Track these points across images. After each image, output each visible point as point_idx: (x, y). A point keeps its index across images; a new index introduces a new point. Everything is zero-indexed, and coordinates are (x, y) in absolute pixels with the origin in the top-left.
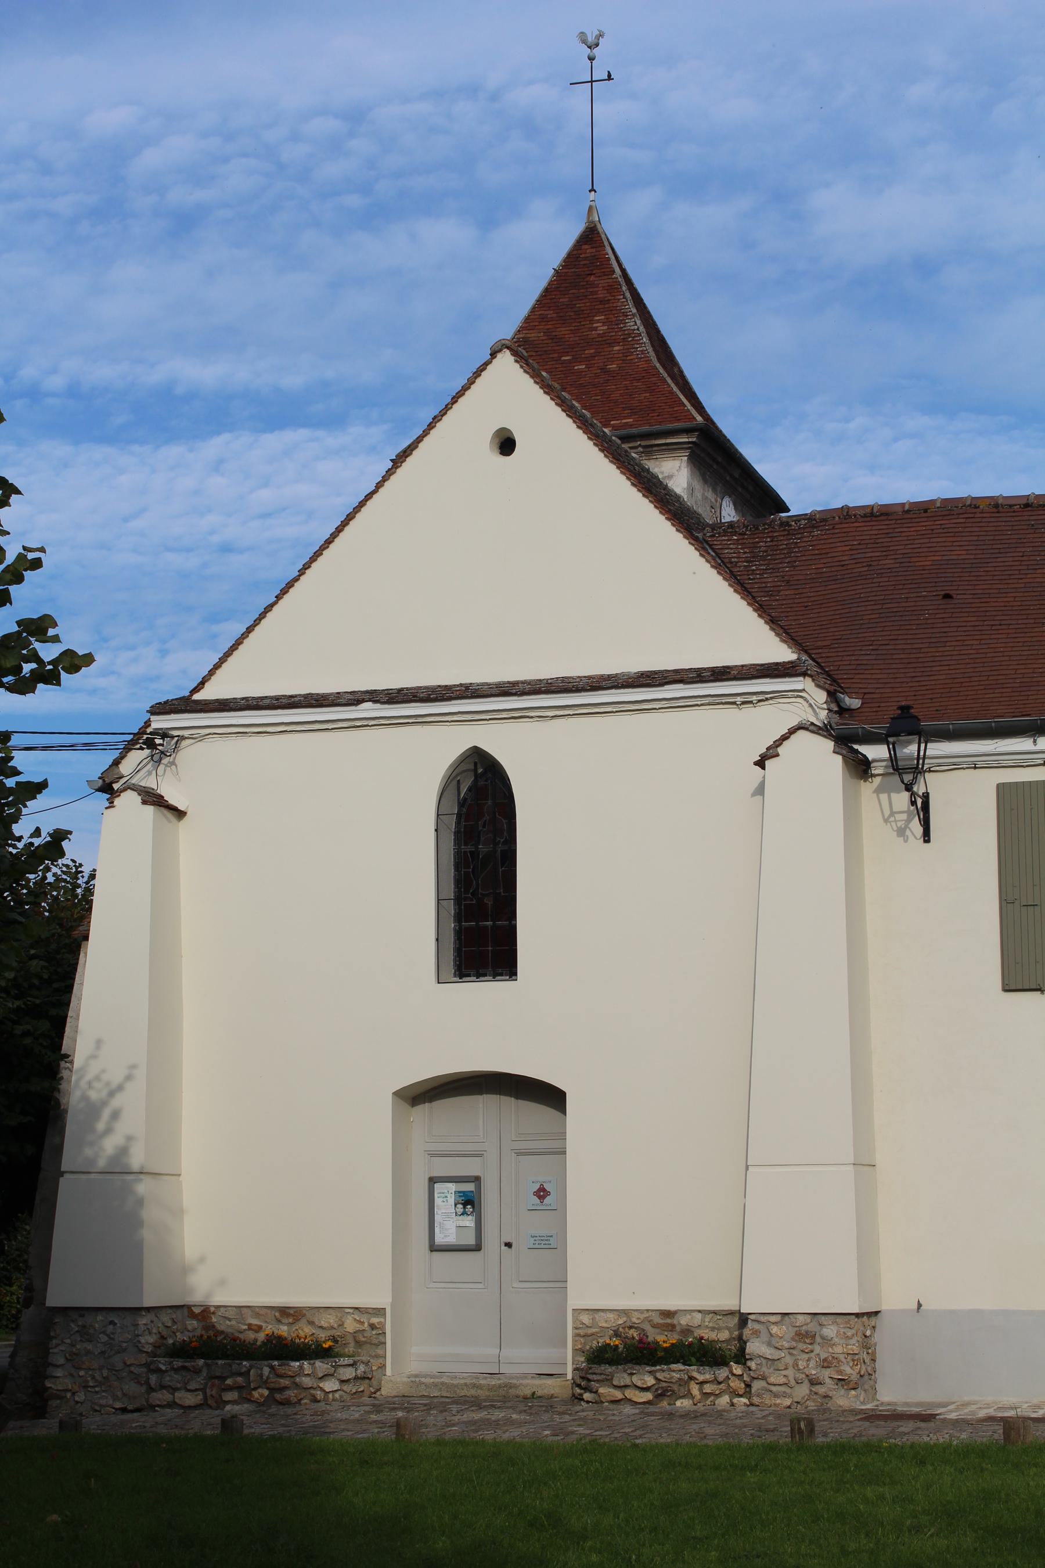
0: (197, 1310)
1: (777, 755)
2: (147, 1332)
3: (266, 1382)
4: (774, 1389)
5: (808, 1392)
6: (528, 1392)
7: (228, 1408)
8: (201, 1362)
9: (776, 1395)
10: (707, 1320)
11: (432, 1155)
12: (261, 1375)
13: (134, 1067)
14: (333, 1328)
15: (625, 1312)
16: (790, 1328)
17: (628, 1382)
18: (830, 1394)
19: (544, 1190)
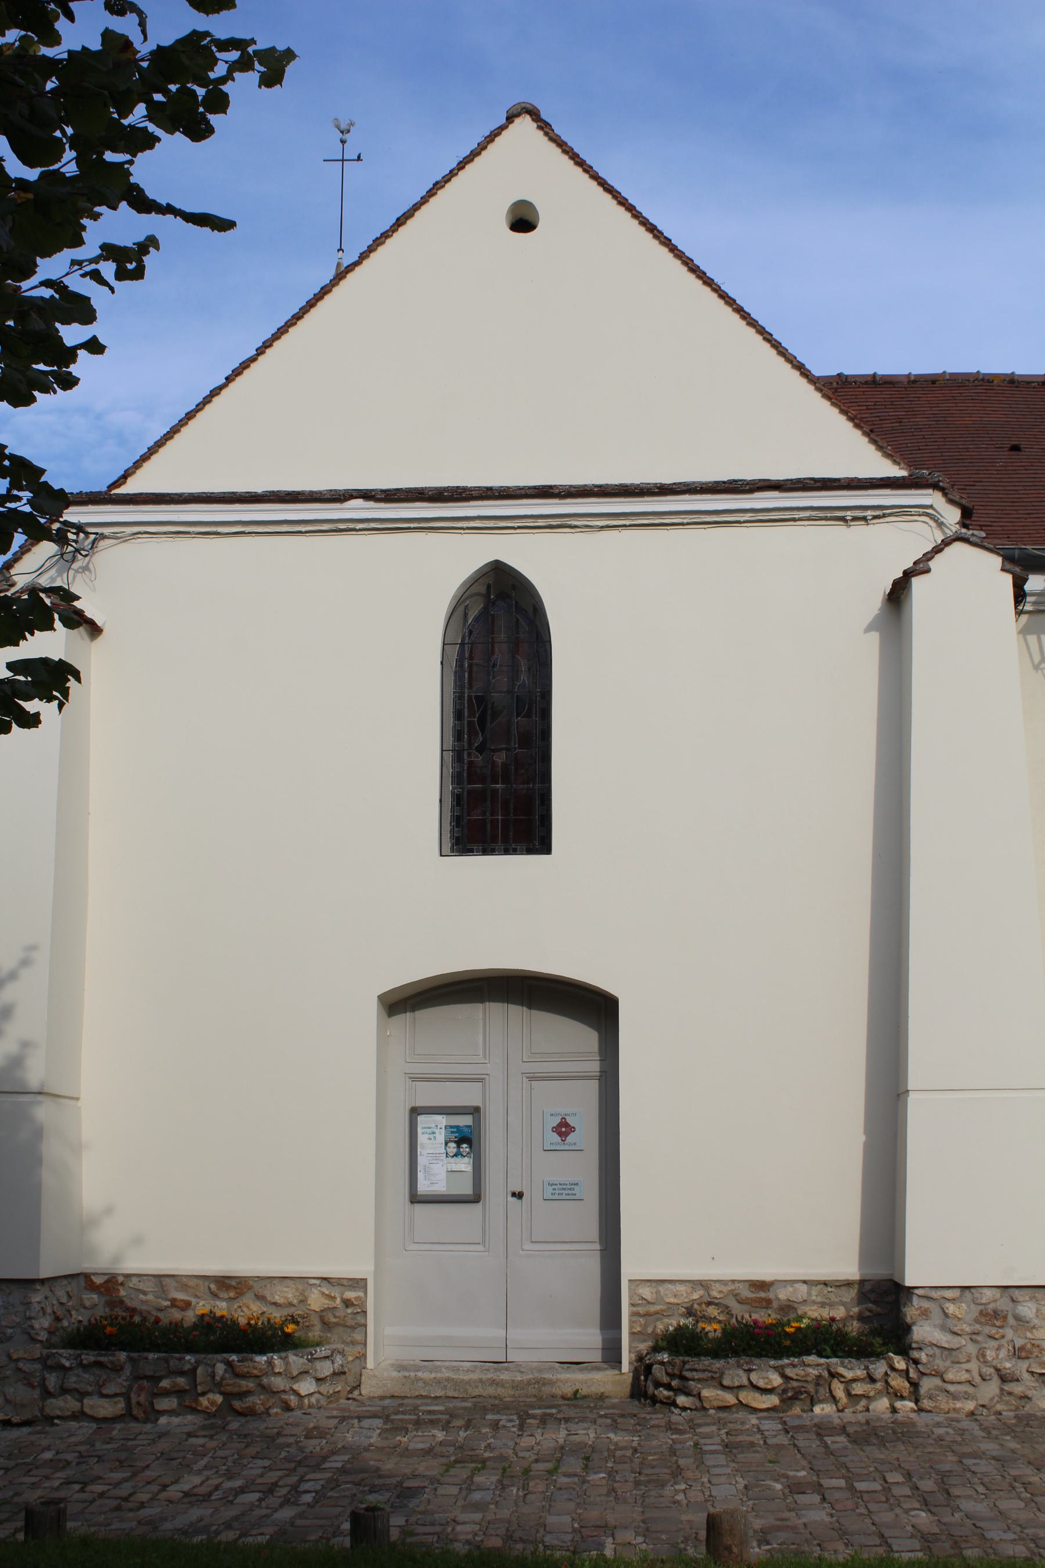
0: (98, 1280)
1: (928, 571)
2: (41, 1314)
3: (220, 1384)
4: (951, 1388)
5: (997, 1391)
6: (568, 1390)
7: (163, 1420)
8: (123, 1356)
9: (955, 1397)
10: (814, 1293)
11: (414, 1079)
12: (213, 1375)
13: (33, 948)
14: (291, 1304)
15: (704, 1284)
16: (972, 1306)
17: (745, 1382)
18: (1029, 1393)
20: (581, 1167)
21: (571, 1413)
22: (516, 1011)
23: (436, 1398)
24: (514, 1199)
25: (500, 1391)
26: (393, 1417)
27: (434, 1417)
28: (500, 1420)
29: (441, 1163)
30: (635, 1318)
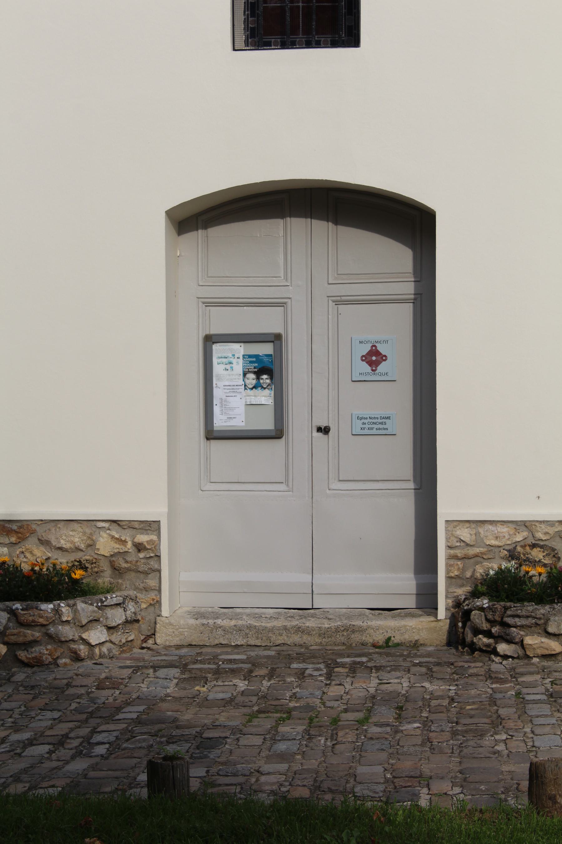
6: (380, 638)
11: (208, 304)
14: (78, 549)
15: (526, 525)
22: (321, 228)
23: (237, 646)
24: (320, 434)
25: (306, 639)
29: (239, 396)
30: (452, 562)
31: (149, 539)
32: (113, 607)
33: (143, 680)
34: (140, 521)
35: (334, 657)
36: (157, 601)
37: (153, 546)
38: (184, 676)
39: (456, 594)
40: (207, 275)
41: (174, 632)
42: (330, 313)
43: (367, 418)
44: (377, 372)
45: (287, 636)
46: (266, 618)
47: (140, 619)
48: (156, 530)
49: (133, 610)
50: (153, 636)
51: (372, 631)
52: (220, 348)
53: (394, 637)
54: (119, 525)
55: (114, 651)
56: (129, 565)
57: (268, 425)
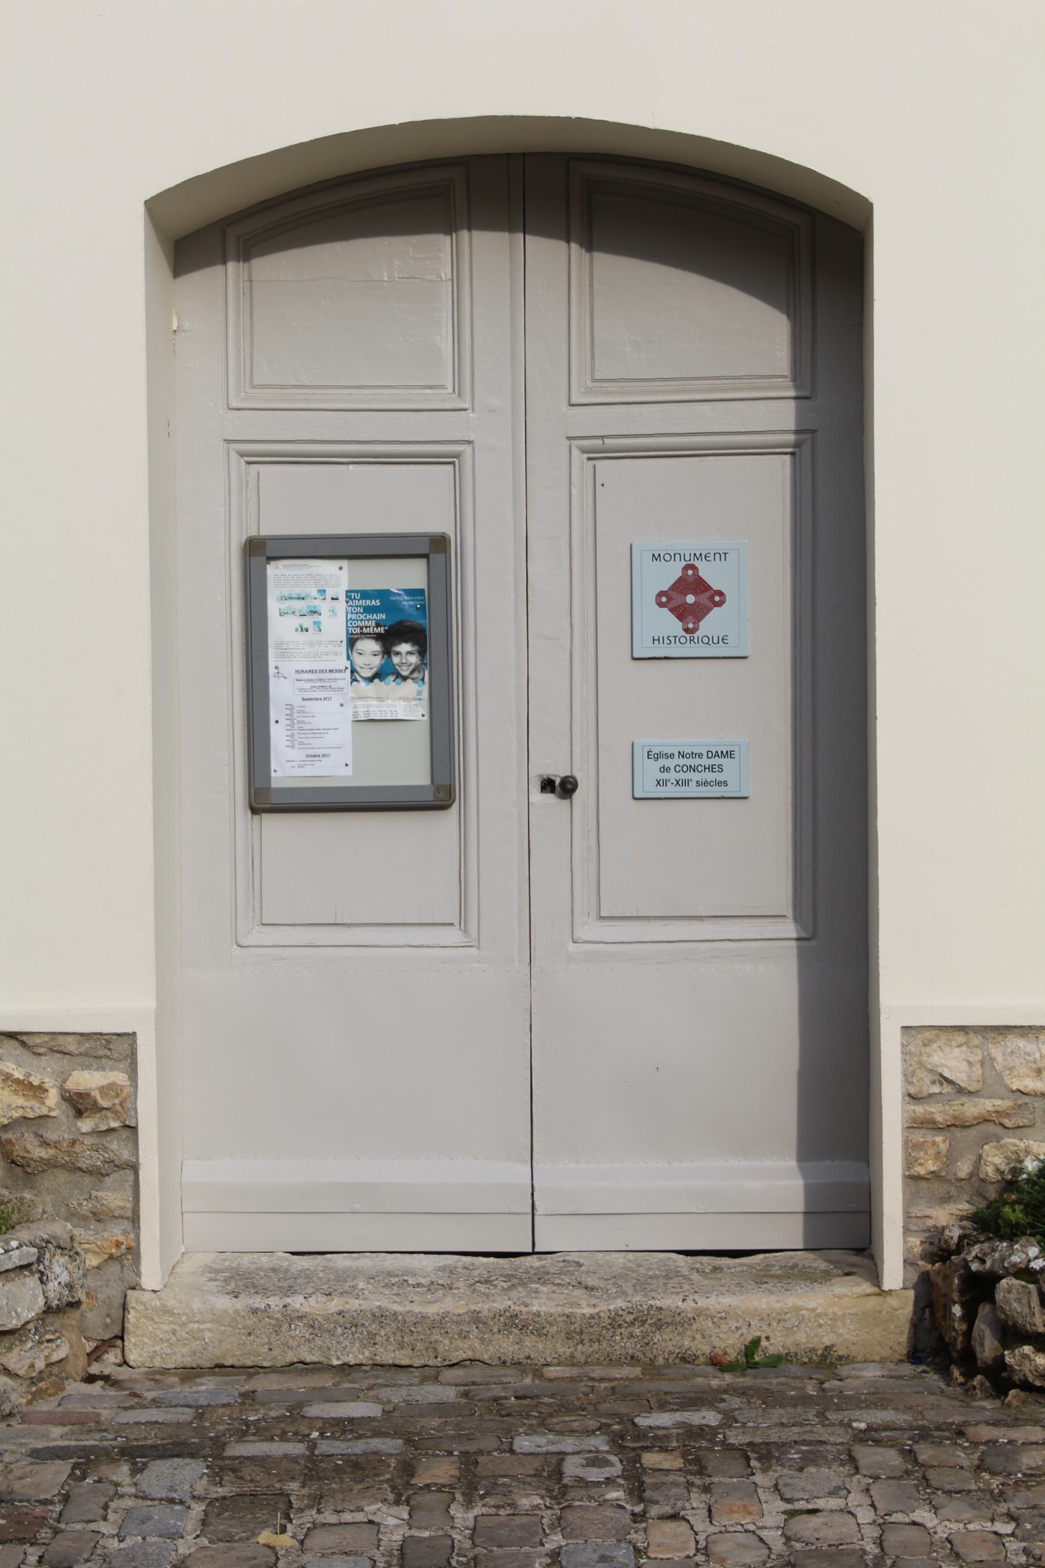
6: (729, 1342)
19: (699, 586)
20: (741, 699)
21: (762, 1425)
22: (550, 259)
23: (346, 1369)
24: (550, 798)
25: (532, 1347)
26: (238, 1449)
27: (359, 1447)
28: (562, 1455)
29: (337, 699)
30: (919, 1137)
31: (105, 1082)
32: (12, 1275)
33: (106, 1507)
34: (82, 1034)
35: (622, 1408)
36: (129, 1249)
37: (117, 1101)
38: (221, 1491)
39: (930, 1223)
40: (251, 381)
41: (174, 1333)
42: (575, 480)
43: (672, 756)
44: (699, 634)
45: (482, 1340)
46: (419, 1285)
47: (83, 1298)
48: (125, 1058)
49: (65, 1278)
50: (119, 1342)
51: (710, 1324)
52: (287, 572)
53: (768, 1338)
54: (23, 1044)
55: (14, 1397)
56: (52, 1152)
57: (413, 772)
